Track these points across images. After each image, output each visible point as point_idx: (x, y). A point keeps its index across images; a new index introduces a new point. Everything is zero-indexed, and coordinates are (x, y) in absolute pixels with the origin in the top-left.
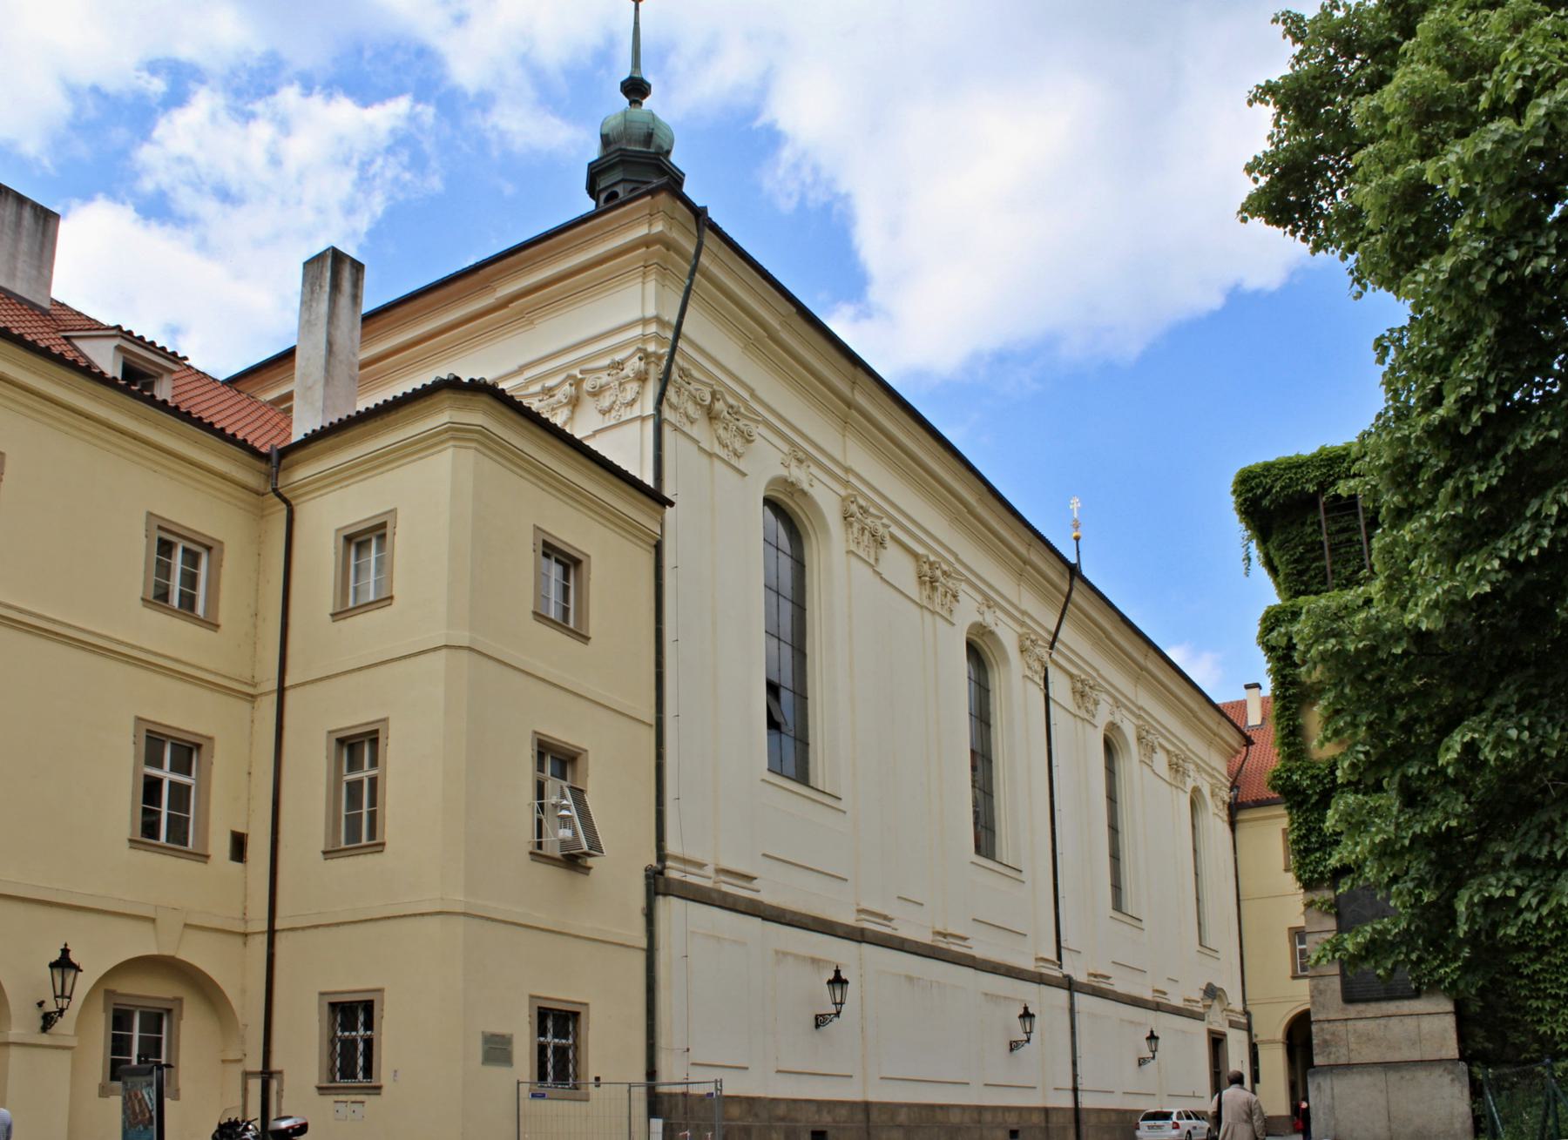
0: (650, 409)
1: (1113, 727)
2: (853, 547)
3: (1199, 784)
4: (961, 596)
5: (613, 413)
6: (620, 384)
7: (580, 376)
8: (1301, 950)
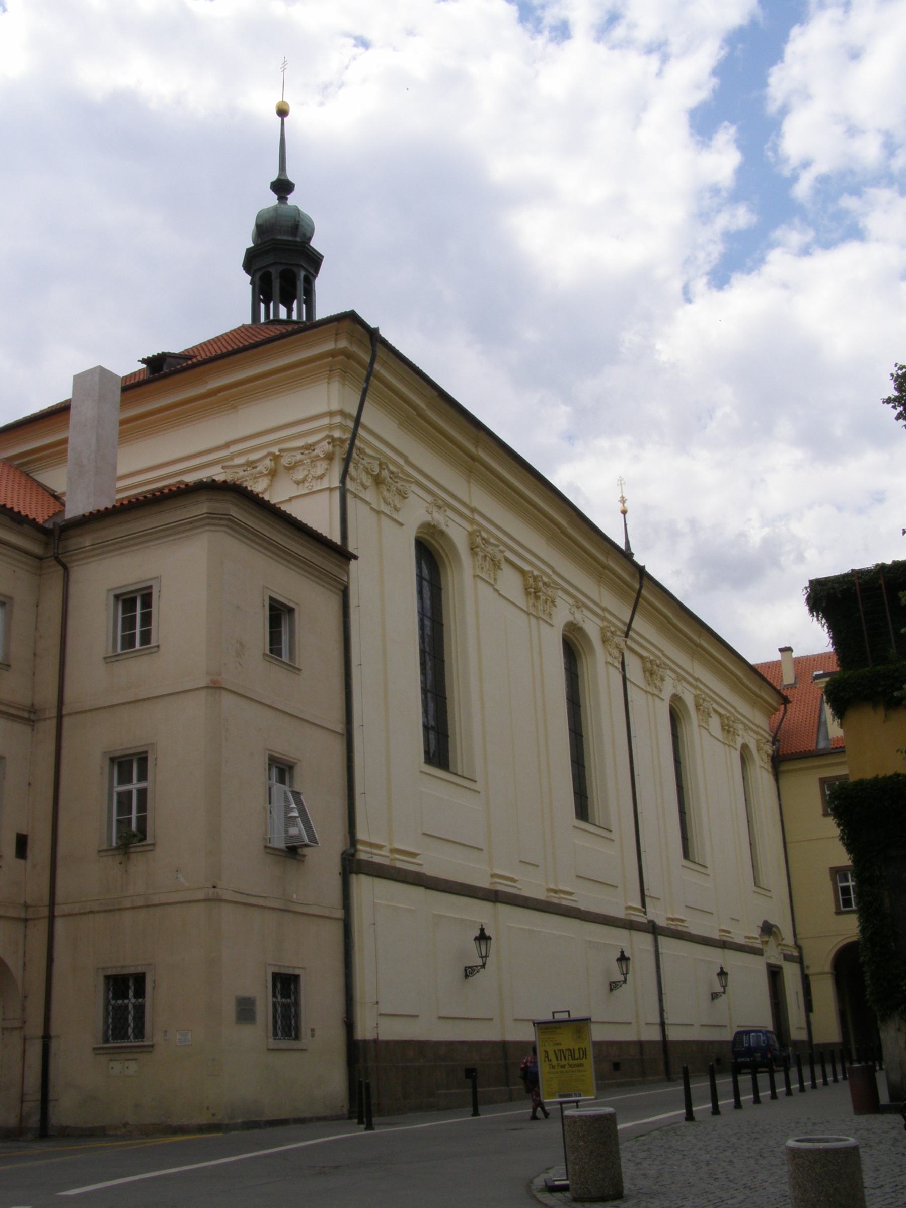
0: (336, 483)
1: (676, 699)
2: (479, 573)
3: (747, 741)
4: (558, 601)
5: (306, 484)
6: (312, 461)
7: (277, 453)
8: (842, 888)
